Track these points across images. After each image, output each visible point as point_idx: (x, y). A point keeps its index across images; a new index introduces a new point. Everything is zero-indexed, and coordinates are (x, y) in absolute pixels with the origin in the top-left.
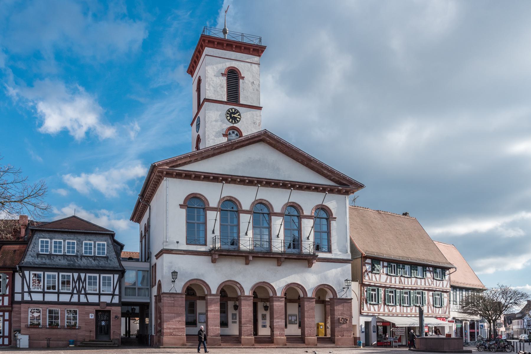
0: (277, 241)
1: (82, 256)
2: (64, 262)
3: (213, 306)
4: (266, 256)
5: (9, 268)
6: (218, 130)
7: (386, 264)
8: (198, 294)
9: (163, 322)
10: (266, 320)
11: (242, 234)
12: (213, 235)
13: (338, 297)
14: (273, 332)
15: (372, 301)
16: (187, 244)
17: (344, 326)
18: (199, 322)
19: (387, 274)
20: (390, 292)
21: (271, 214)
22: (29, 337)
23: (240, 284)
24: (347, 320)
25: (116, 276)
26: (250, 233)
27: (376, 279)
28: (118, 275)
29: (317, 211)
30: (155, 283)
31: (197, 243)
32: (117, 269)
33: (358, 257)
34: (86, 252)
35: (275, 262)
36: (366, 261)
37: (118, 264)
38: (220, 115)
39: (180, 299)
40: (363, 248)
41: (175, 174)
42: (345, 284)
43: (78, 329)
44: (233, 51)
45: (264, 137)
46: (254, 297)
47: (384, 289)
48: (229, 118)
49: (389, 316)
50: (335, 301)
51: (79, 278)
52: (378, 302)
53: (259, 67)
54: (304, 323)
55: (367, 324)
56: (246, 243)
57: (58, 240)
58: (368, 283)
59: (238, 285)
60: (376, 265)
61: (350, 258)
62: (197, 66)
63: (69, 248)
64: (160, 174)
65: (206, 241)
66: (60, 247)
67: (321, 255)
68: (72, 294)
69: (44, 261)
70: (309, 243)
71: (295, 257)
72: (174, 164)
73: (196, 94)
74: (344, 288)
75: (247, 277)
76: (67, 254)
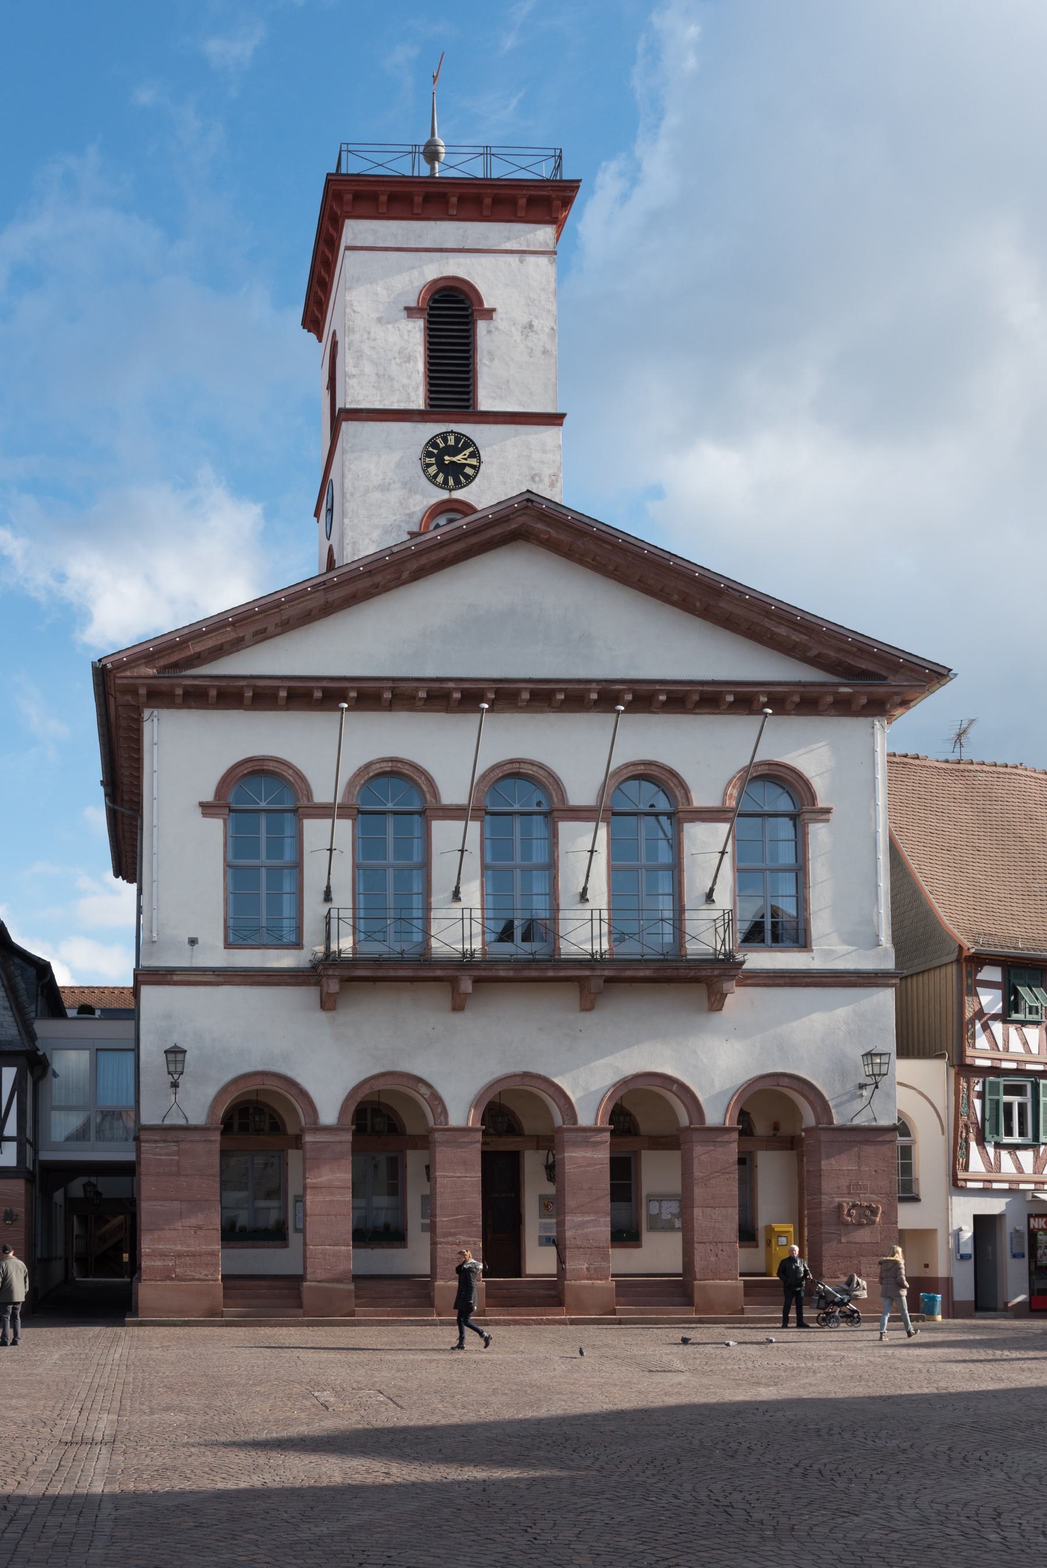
0: (579, 914)
4: (526, 973)
8: (529, 1126)
11: (440, 896)
13: (837, 1121)
15: (1009, 1132)
16: (228, 945)
17: (864, 1235)
21: (680, 813)
24: (874, 1212)
27: (1025, 1043)
32: (11, 1048)
35: (571, 996)
36: (980, 976)
38: (399, 465)
45: (522, 519)
46: (742, 1133)
48: (433, 470)
50: (825, 1137)
52: (1036, 1137)
55: (981, 1222)
56: (583, 933)
58: (988, 1063)
60: (1023, 990)
61: (890, 964)
64: (129, 698)
65: (299, 929)
71: (648, 973)
72: (175, 657)
74: (862, 1086)
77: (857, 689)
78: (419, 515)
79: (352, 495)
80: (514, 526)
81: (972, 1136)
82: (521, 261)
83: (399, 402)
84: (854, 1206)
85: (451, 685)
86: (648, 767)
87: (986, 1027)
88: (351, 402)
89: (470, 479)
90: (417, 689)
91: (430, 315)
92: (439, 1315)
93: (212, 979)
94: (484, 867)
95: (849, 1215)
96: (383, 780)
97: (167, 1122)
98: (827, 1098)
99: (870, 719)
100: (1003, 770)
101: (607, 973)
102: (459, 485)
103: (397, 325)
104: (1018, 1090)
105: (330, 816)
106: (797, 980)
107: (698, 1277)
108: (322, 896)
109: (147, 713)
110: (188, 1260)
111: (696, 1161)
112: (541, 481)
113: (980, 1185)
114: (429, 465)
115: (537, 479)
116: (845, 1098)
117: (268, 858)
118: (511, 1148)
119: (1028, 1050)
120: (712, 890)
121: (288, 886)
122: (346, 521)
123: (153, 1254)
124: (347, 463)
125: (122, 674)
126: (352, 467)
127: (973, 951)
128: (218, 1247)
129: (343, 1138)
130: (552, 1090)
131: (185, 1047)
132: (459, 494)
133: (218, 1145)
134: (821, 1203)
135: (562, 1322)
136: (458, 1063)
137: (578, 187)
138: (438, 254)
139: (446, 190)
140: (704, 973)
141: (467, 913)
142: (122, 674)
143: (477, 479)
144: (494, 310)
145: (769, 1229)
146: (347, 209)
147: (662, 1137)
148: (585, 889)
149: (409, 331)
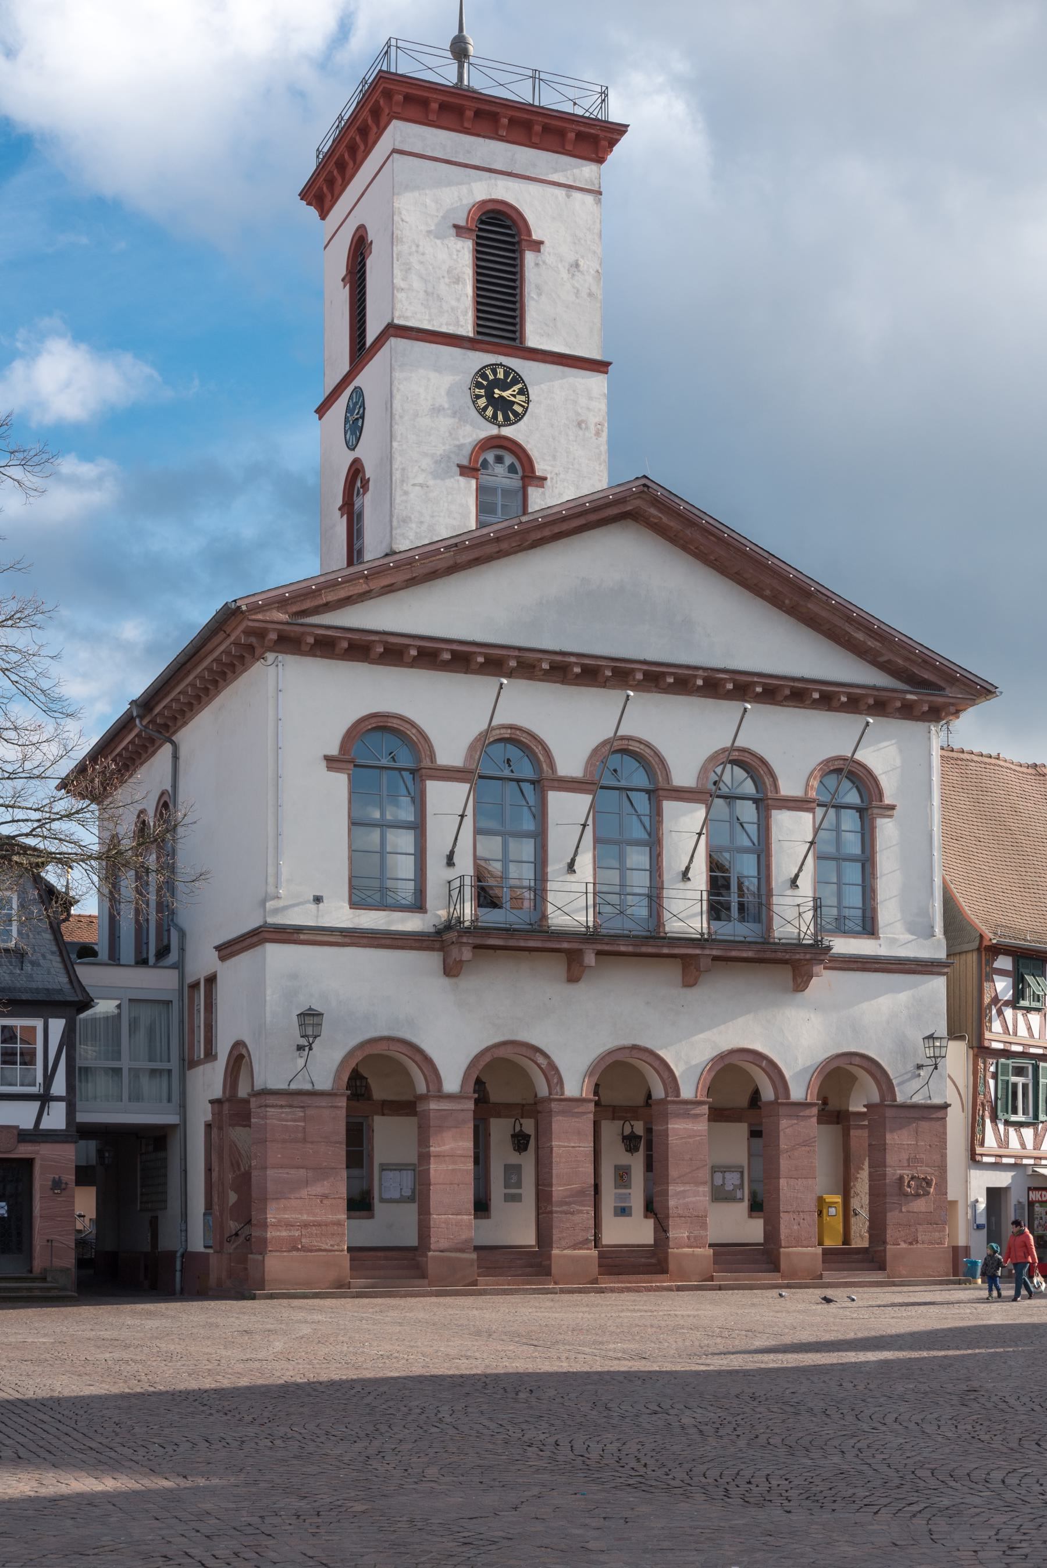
4: (644, 949)
6: (440, 450)
9: (264, 1200)
10: (628, 1186)
11: (555, 867)
12: (451, 874)
13: (900, 1099)
14: (666, 1231)
15: (1015, 1111)
17: (920, 1205)
18: (382, 1200)
21: (660, 790)
24: (929, 1184)
25: (57, 1026)
26: (585, 862)
27: (1029, 1028)
29: (832, 781)
30: (210, 1055)
32: (60, 998)
33: (966, 947)
35: (675, 972)
36: (996, 965)
37: (64, 979)
40: (986, 917)
41: (311, 640)
42: (924, 1053)
44: (501, 139)
45: (638, 502)
48: (482, 402)
50: (889, 1113)
52: (1036, 1116)
53: (598, 202)
54: (778, 1199)
55: (994, 1195)
56: (571, 903)
58: (1000, 1046)
59: (541, 1060)
61: (941, 954)
62: (346, 183)
65: (420, 892)
67: (842, 946)
70: (799, 901)
71: (750, 954)
72: (308, 604)
73: (342, 296)
74: (920, 1067)
75: (574, 1031)
77: (921, 697)
78: (469, 449)
79: (401, 417)
80: (629, 508)
81: (987, 1113)
82: (568, 196)
83: (447, 324)
85: (573, 659)
86: (741, 753)
88: (399, 317)
89: (519, 417)
90: (540, 660)
91: (478, 237)
92: (556, 1283)
93: (339, 939)
95: (909, 1186)
98: (892, 1077)
99: (927, 724)
101: (715, 953)
102: (507, 422)
103: (446, 241)
104: (1019, 1071)
106: (868, 966)
107: (783, 1244)
108: (445, 861)
110: (314, 1230)
111: (781, 1134)
112: (587, 428)
114: (478, 397)
115: (583, 425)
116: (906, 1077)
119: (1032, 1035)
120: (797, 876)
122: (395, 444)
124: (396, 383)
125: (253, 617)
126: (401, 387)
127: (994, 941)
128: (344, 1217)
129: (465, 1107)
130: (656, 1064)
131: (320, 1010)
132: (507, 431)
133: (344, 1111)
134: (885, 1175)
135: (669, 1289)
137: (625, 132)
138: (487, 174)
139: (498, 110)
140: (798, 957)
142: (253, 617)
143: (525, 418)
144: (542, 243)
147: (726, 1109)
148: (688, 868)
149: (458, 251)
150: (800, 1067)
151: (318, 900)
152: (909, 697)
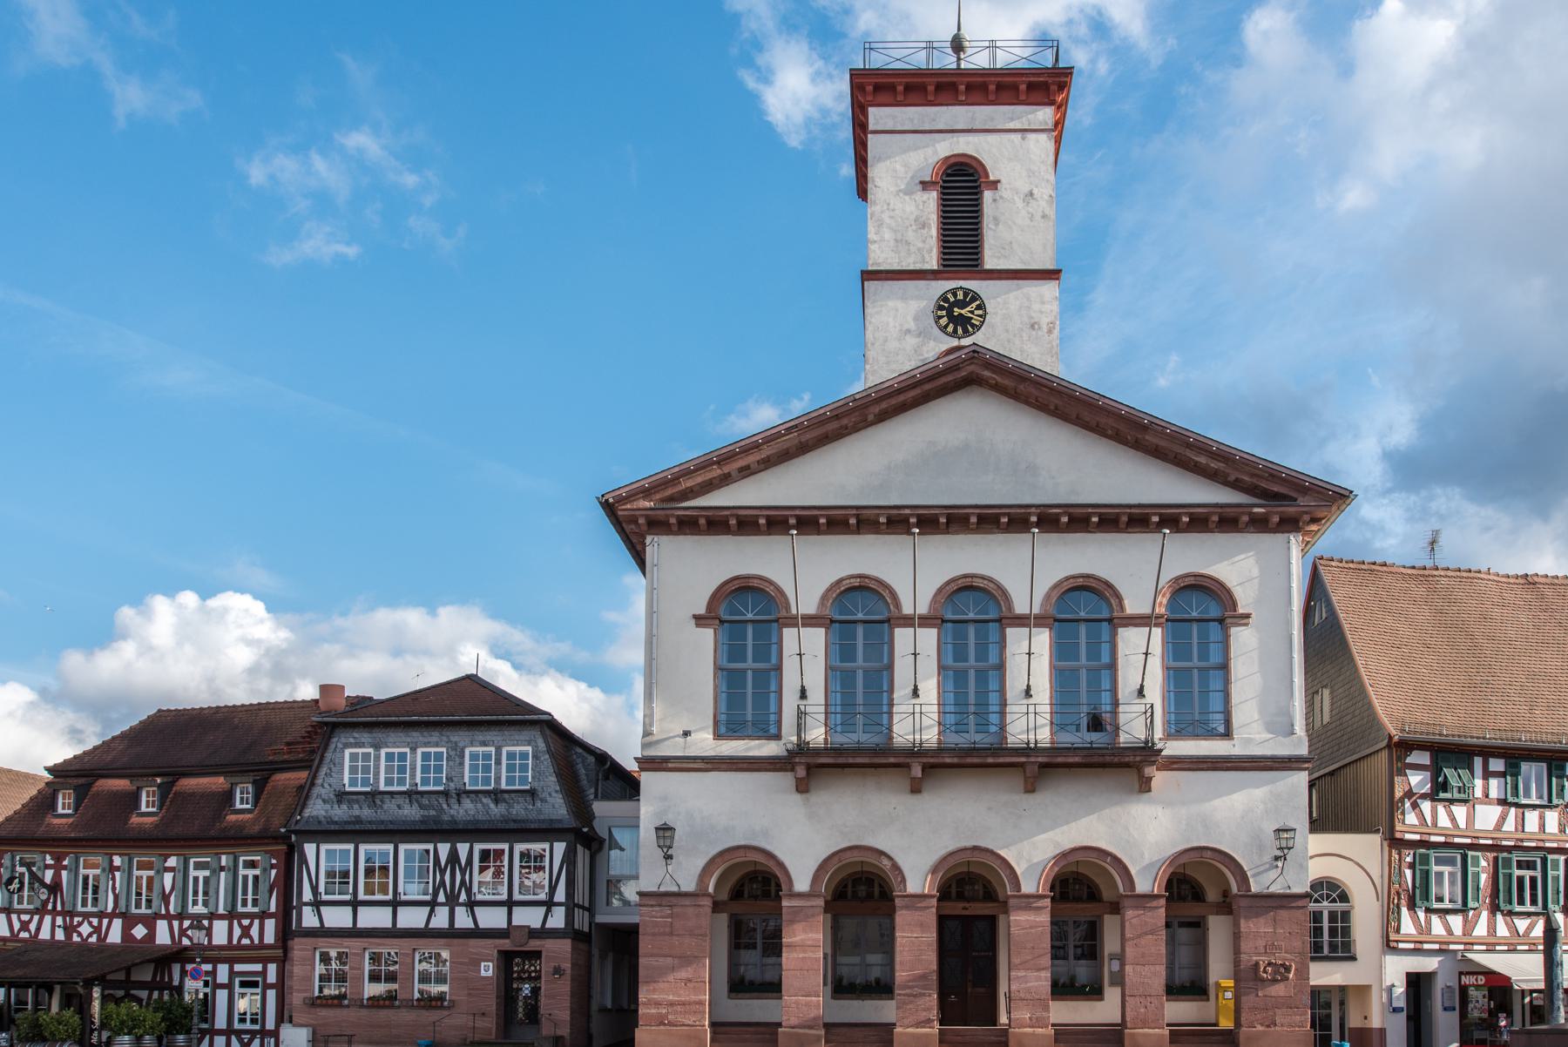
1: (462, 793)
2: (411, 812)
3: (798, 927)
4: (969, 760)
5: (277, 838)
7: (1497, 765)
8: (1212, 895)
11: (901, 692)
13: (1254, 889)
15: (1521, 902)
16: (718, 736)
17: (1278, 990)
19: (1503, 802)
20: (1520, 865)
22: (314, 1033)
23: (890, 858)
24: (1288, 969)
25: (560, 848)
28: (564, 844)
31: (1200, 731)
34: (474, 780)
35: (1018, 781)
39: (691, 910)
43: (448, 1008)
44: (962, 103)
46: (1168, 899)
47: (1490, 855)
48: (944, 321)
49: (1514, 951)
51: (453, 857)
55: (1417, 984)
57: (396, 750)
58: (1417, 837)
61: (1303, 751)
63: (425, 769)
65: (779, 722)
66: (402, 770)
68: (432, 904)
69: (356, 811)
71: (1077, 759)
72: (669, 492)
74: (1277, 858)
76: (420, 788)
84: (1270, 964)
85: (907, 511)
87: (1415, 806)
89: (977, 328)
94: (942, 668)
96: (850, 595)
97: (662, 889)
100: (1467, 576)
102: (966, 333)
104: (1530, 865)
105: (1028, 625)
109: (649, 539)
110: (679, 1008)
113: (1411, 946)
114: (941, 317)
117: (955, 661)
118: (987, 912)
121: (993, 685)
123: (650, 1003)
136: (916, 838)
141: (1031, 709)
145: (1217, 985)
146: (870, 98)
150: (1147, 861)
151: (686, 734)
152: (1256, 510)
